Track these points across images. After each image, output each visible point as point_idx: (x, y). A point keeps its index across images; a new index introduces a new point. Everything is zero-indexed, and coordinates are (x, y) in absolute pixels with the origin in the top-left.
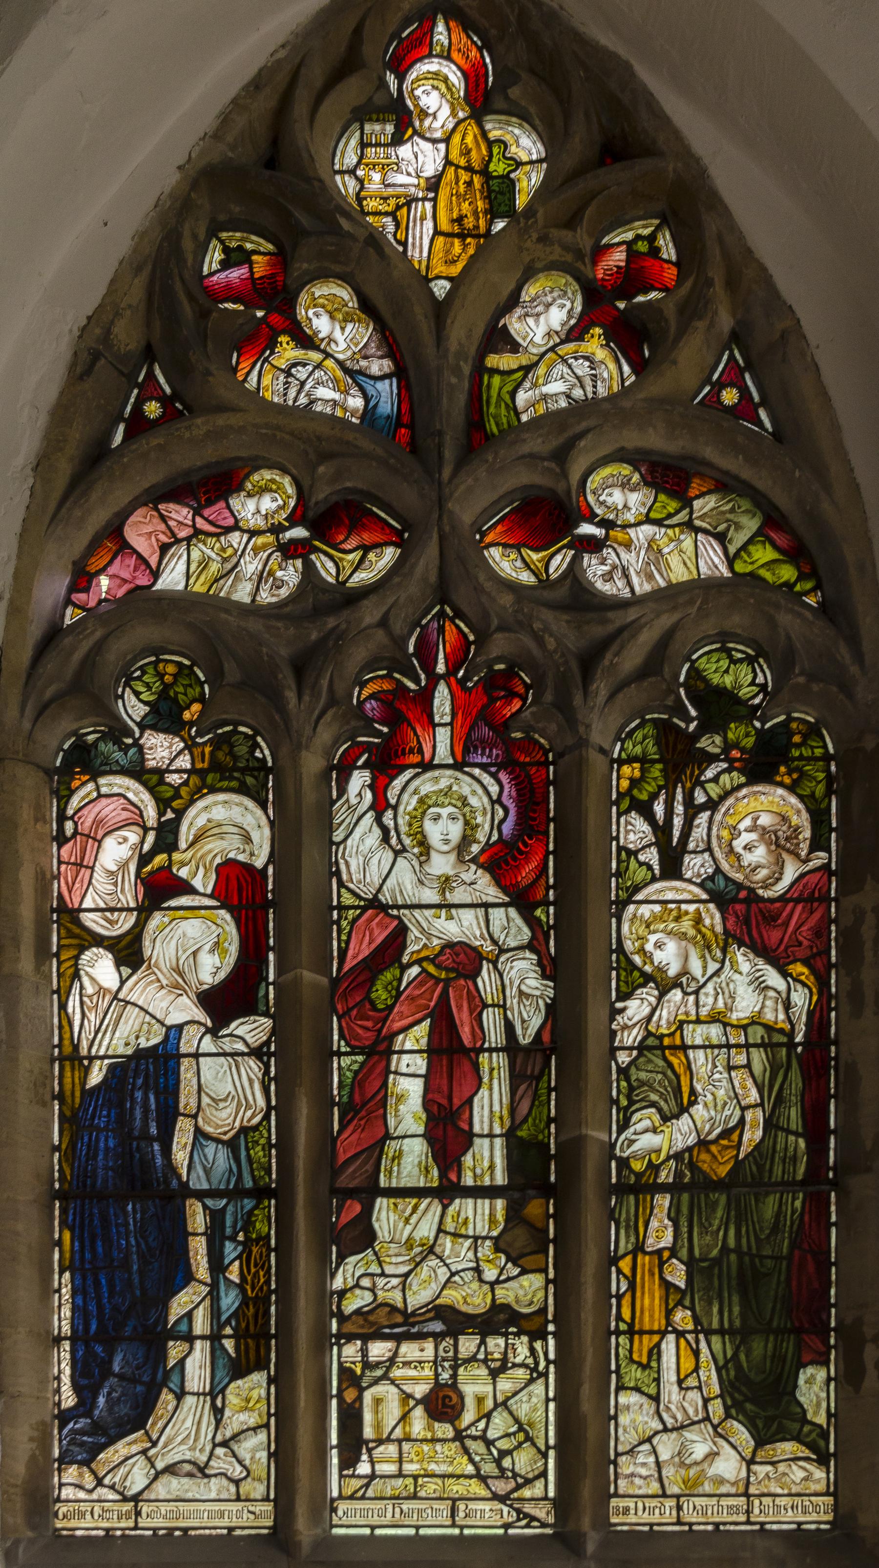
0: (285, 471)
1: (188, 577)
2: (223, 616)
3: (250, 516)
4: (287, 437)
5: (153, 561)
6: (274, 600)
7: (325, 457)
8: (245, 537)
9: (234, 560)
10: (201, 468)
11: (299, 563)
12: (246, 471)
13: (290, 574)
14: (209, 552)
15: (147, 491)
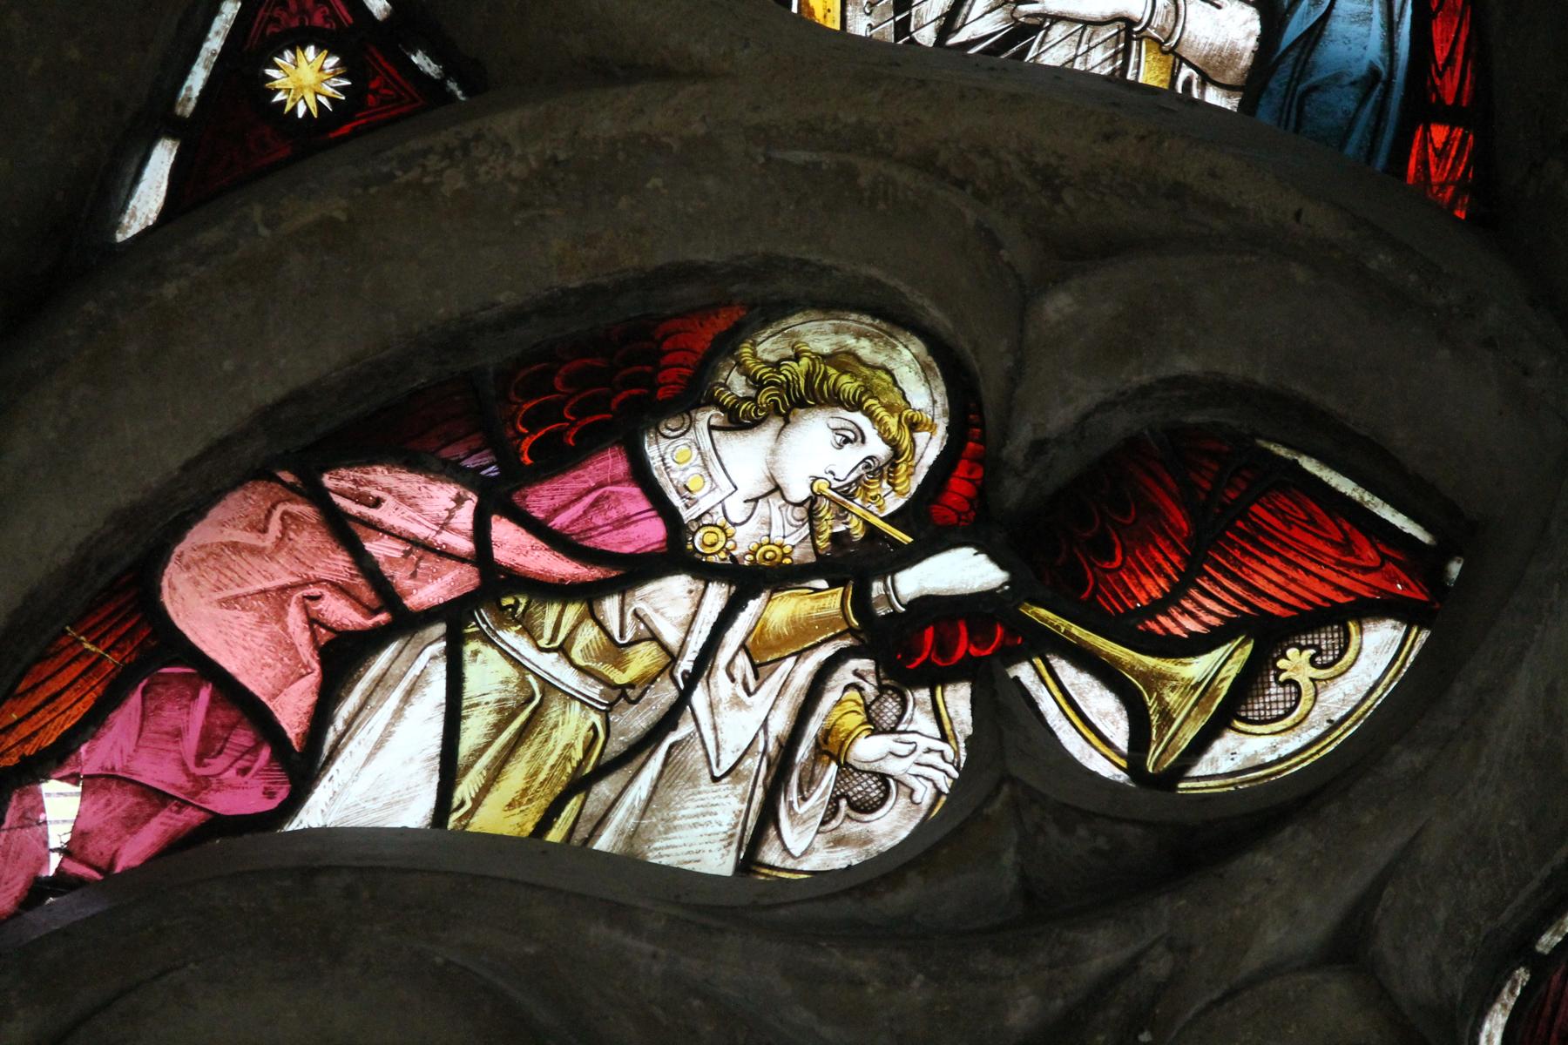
0: (895, 317)
1: (449, 768)
2: (598, 931)
3: (737, 510)
4: (904, 177)
5: (291, 712)
6: (841, 858)
7: (1072, 254)
8: (717, 595)
9: (665, 694)
10: (517, 317)
11: (958, 700)
12: (722, 322)
13: (920, 750)
14: (550, 665)
15: (267, 417)
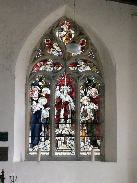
13: (52, 69)
